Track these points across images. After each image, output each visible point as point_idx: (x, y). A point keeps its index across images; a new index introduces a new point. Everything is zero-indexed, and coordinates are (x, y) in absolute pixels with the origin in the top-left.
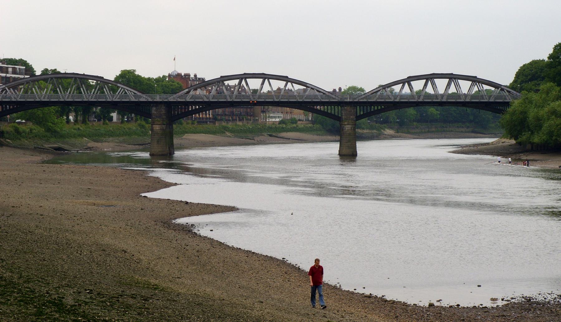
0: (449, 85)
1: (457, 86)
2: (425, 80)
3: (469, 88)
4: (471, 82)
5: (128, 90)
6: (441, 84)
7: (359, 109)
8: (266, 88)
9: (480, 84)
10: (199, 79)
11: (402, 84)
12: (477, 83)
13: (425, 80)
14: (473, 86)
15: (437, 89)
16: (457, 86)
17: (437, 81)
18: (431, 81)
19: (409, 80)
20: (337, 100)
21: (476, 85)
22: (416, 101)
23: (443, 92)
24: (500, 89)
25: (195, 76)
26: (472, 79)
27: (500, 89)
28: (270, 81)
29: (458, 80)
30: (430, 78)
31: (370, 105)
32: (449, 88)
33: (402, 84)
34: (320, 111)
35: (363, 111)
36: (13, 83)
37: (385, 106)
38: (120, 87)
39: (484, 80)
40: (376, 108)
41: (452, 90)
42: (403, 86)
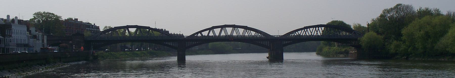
6: (229, 30)
11: (209, 30)
18: (245, 35)
25: (165, 30)
30: (223, 27)
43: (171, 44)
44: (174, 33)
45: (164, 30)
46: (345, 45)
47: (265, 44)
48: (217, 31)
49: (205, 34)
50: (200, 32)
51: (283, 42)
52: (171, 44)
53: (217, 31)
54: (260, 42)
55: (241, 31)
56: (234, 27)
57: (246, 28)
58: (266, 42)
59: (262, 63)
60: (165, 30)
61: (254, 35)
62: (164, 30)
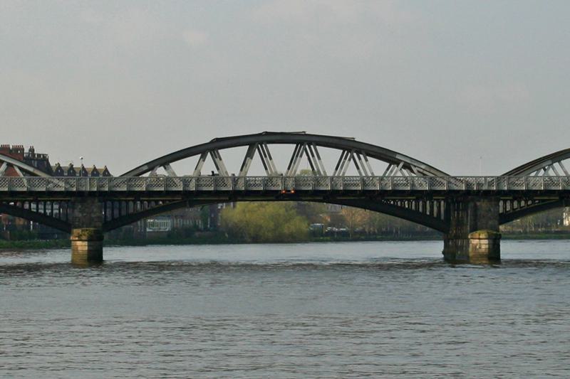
0: (296, 156)
1: (313, 156)
2: (248, 147)
3: (320, 154)
4: (342, 151)
5: (21, 169)
6: (281, 154)
7: (240, 205)
8: (350, 170)
9: (361, 156)
10: (39, 155)
11: (200, 155)
12: (355, 154)
13: (248, 147)
14: (297, 156)
15: (272, 162)
16: (313, 156)
17: (273, 148)
18: (259, 149)
19: (213, 147)
20: (63, 189)
21: (352, 160)
22: (25, 189)
23: (118, 176)
24: (401, 165)
25: (32, 150)
26: (297, 138)
27: (401, 165)
28: (221, 154)
29: (268, 145)
30: (256, 142)
31: (511, 198)
32: (220, 159)
33: (200, 155)
34: (409, 210)
35: (120, 210)
36: (5, 160)
37: (166, 200)
38: (402, 161)
39: (336, 140)
40: (523, 203)
41: (303, 165)
42: (250, 155)
43: (45, 209)
44: (72, 166)
45: (26, 150)
46: (32, 199)
47: (421, 210)
48: (232, 159)
49: (184, 168)
50: (165, 161)
51: (442, 218)
52: (45, 209)
53: (232, 159)
54: (41, 206)
55: (329, 159)
56: (302, 141)
57: (348, 146)
58: (432, 211)
59: (430, 265)
60: (32, 150)
61: (381, 175)
62: (26, 150)
